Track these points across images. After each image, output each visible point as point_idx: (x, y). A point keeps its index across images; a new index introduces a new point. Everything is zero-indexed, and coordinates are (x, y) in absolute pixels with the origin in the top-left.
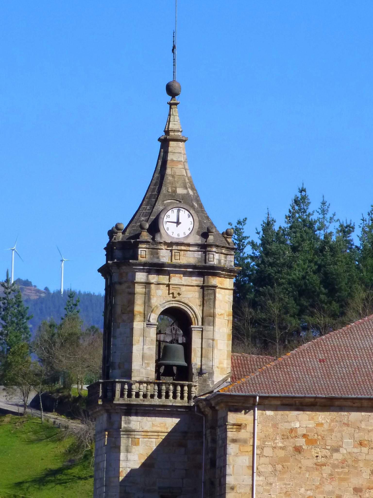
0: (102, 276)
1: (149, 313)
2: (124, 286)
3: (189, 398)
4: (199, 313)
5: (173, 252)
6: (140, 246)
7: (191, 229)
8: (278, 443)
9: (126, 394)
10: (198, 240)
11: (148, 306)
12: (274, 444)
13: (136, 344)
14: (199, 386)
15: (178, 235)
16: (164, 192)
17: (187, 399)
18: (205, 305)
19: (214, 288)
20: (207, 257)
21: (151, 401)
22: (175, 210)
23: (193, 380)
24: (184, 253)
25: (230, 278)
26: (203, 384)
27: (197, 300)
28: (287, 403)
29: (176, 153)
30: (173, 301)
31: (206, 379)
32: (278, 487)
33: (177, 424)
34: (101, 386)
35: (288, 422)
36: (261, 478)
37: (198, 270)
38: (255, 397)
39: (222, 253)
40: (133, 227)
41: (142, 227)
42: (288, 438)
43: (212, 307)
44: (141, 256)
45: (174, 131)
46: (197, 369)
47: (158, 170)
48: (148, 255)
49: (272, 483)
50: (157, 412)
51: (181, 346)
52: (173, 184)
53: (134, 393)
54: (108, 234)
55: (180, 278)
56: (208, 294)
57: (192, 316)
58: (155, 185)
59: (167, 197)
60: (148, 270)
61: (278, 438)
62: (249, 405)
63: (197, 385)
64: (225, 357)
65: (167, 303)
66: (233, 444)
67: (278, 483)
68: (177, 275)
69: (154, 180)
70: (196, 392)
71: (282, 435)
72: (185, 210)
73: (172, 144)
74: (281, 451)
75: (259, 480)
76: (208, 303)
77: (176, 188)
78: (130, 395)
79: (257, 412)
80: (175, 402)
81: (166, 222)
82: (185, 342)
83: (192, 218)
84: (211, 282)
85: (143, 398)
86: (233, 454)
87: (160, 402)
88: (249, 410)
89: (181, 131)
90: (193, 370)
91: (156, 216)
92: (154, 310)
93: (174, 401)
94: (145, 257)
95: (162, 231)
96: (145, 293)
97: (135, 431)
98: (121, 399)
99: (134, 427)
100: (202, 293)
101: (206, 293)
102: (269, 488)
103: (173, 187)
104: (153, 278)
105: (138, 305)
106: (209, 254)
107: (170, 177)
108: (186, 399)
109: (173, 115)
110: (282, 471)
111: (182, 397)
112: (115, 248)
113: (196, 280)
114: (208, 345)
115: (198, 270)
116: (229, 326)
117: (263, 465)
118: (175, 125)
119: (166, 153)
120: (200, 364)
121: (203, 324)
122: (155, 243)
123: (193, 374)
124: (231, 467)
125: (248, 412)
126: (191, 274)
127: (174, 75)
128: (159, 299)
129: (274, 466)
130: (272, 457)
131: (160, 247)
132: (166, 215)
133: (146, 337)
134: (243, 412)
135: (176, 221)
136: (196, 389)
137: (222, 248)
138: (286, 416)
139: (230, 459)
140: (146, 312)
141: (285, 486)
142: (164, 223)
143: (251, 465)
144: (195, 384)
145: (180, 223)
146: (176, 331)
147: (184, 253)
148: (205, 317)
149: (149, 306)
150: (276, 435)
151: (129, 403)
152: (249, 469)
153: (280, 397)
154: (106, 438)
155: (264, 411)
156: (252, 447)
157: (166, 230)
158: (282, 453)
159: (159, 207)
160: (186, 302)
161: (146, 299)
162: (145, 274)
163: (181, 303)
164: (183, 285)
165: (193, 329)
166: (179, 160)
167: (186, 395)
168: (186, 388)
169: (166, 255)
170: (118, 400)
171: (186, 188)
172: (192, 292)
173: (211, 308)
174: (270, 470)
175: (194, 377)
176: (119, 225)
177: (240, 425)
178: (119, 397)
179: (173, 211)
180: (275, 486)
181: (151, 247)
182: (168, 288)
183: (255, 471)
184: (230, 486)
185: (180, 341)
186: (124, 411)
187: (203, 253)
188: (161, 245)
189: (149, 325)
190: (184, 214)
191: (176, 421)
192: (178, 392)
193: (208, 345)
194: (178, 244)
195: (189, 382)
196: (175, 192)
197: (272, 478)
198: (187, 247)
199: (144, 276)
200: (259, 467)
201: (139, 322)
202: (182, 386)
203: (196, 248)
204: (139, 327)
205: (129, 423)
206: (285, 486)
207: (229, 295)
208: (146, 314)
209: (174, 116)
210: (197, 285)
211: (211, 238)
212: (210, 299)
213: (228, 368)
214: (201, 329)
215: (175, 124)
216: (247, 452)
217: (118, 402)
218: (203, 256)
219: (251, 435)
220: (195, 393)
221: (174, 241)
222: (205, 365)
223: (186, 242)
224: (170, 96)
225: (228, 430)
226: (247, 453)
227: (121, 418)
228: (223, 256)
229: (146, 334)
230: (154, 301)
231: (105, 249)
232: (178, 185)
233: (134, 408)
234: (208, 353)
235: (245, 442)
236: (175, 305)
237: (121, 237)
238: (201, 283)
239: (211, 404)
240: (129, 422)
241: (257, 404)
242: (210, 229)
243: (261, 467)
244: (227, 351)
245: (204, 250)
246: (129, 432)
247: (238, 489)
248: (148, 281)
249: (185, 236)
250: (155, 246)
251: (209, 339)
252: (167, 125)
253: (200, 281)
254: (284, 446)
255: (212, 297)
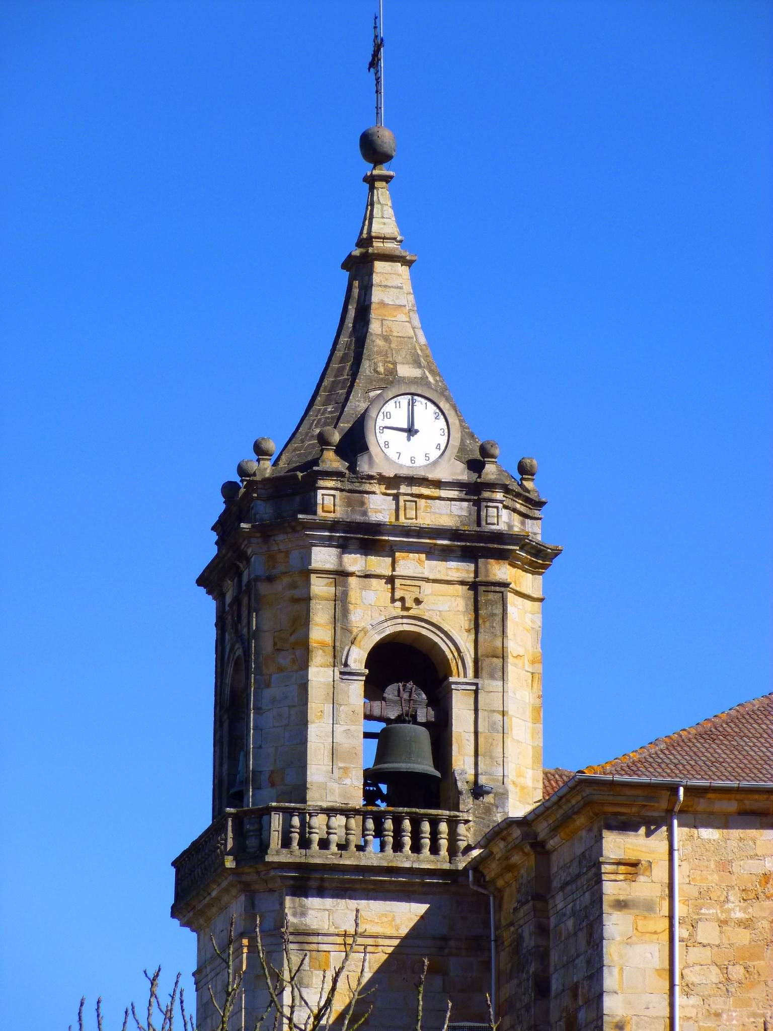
0: (209, 593)
1: (345, 646)
2: (279, 586)
3: (453, 851)
4: (467, 648)
5: (402, 499)
6: (321, 483)
7: (443, 448)
8: (733, 909)
9: (295, 838)
10: (461, 473)
11: (342, 628)
12: (722, 912)
13: (316, 721)
14: (474, 822)
15: (412, 460)
16: (367, 371)
17: (447, 853)
18: (481, 630)
19: (502, 589)
20: (483, 514)
21: (359, 858)
22: (404, 400)
23: (461, 807)
24: (426, 503)
25: (533, 573)
26: (484, 819)
27: (462, 617)
28: (756, 806)
29: (390, 287)
30: (403, 617)
31: (491, 806)
32: (734, 1022)
33: (422, 917)
34: (230, 823)
35: (755, 857)
36: (693, 1000)
37: (464, 544)
38: (674, 789)
39: (515, 510)
40: (295, 450)
41: (323, 440)
42: (758, 898)
43: (499, 632)
44: (323, 508)
45: (384, 238)
46: (467, 782)
47: (348, 328)
48: (340, 507)
49: (720, 1011)
50: (372, 887)
51: (424, 728)
52: (386, 355)
53: (315, 838)
54: (222, 492)
55: (420, 561)
56: (487, 602)
57: (450, 656)
58: (343, 359)
59: (374, 383)
60: (341, 541)
61: (732, 898)
62: (655, 814)
63: (470, 819)
64: (529, 761)
65: (389, 623)
66: (619, 913)
67: (736, 1011)
68: (411, 555)
69: (339, 351)
70: (469, 835)
71: (743, 890)
72: (426, 401)
73: (379, 266)
74: (741, 930)
75: (688, 1006)
76: (487, 624)
77: (395, 364)
78: (305, 843)
79: (679, 832)
80: (418, 860)
81: (381, 428)
82: (433, 719)
83: (444, 420)
84: (495, 575)
85: (338, 850)
86: (618, 938)
87: (381, 858)
88: (658, 827)
89: (401, 241)
90: (459, 784)
91: (352, 423)
92: (358, 639)
93: (415, 858)
94: (334, 510)
95: (373, 448)
96: (336, 596)
97: (318, 934)
98: (284, 851)
99: (315, 924)
100: (473, 600)
101: (482, 599)
102: (714, 1025)
103: (389, 362)
104: (354, 562)
105: (317, 625)
106: (487, 507)
107: (380, 339)
108: (444, 852)
109: (379, 202)
110: (743, 981)
111: (434, 850)
112: (255, 495)
113: (458, 569)
114: (492, 727)
115: (464, 544)
116: (535, 685)
117: (697, 968)
118: (385, 226)
119: (367, 288)
120: (473, 772)
121: (476, 675)
122: (357, 478)
123: (460, 793)
124: (616, 971)
125: (655, 830)
126: (444, 554)
127: (377, 113)
128: (369, 612)
129: (724, 969)
130: (718, 946)
131: (367, 487)
132: (382, 411)
133: (341, 705)
134: (643, 830)
135: (405, 426)
136: (468, 830)
137: (514, 499)
138: (751, 843)
139: (612, 951)
140: (338, 644)
141: (752, 1020)
142: (377, 431)
143: (667, 966)
144: (465, 816)
145: (417, 431)
146: (411, 693)
147: (426, 503)
148: (482, 656)
149: (346, 630)
150: (728, 890)
151: (303, 860)
152: (660, 976)
153: (739, 790)
154: (245, 955)
155: (695, 827)
156: (667, 921)
157: (383, 448)
158: (743, 937)
159: (357, 403)
160: (434, 621)
161: (337, 610)
162: (334, 551)
163: (423, 624)
164: (427, 580)
165: (453, 687)
166: (398, 302)
167: (444, 843)
168: (443, 827)
169: (383, 507)
170: (276, 854)
171: (419, 366)
172: (449, 598)
173: (496, 635)
174: (715, 980)
175: (464, 800)
176: (263, 442)
177: (635, 865)
178: (280, 846)
179: (399, 402)
180: (727, 1021)
181: (347, 488)
182: (389, 586)
183: (677, 980)
184: (615, 1021)
185: (421, 718)
186: (292, 882)
187: (473, 505)
188: (370, 483)
189: (347, 674)
190: (425, 412)
191: (420, 909)
192: (423, 835)
193: (492, 727)
194: (412, 480)
195: (452, 812)
196: (393, 372)
197: (720, 1000)
198: (433, 490)
199: (332, 557)
200: (685, 972)
201: (321, 667)
202: (434, 823)
203: (456, 493)
204: (322, 680)
205: (303, 914)
206: (752, 1020)
207: (532, 614)
208: (338, 648)
209: (382, 205)
210: (460, 579)
211: (490, 471)
212: (493, 615)
213: (535, 789)
214: (474, 688)
215: (384, 224)
216: (655, 933)
217: (276, 859)
218: (472, 513)
219: (663, 891)
220: (465, 839)
221: (403, 472)
222: (486, 773)
223: (431, 476)
224: (371, 163)
225: (604, 877)
226: (655, 936)
227: (282, 904)
228: (516, 518)
229: (340, 698)
230: (358, 618)
231: (213, 529)
232: (399, 359)
233: (317, 875)
234: (491, 745)
235: (649, 907)
236: (407, 627)
237: (268, 471)
238: (470, 577)
239: (536, 835)
240: (302, 913)
241: (677, 808)
242: (488, 446)
243: (691, 971)
244: (533, 747)
245: (476, 498)
246: (304, 935)
247: (634, 1027)
248: (340, 569)
249: (428, 462)
250: (356, 486)
251: (494, 711)
252: (366, 227)
253: (468, 572)
254: (747, 917)
255: (498, 611)
